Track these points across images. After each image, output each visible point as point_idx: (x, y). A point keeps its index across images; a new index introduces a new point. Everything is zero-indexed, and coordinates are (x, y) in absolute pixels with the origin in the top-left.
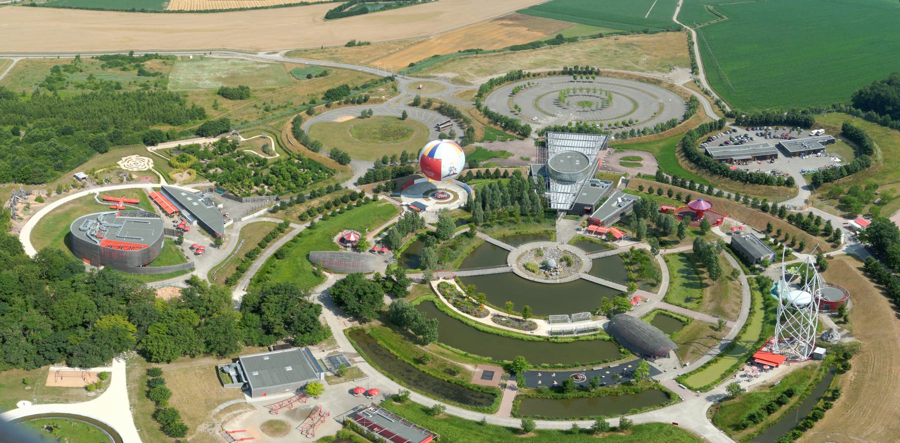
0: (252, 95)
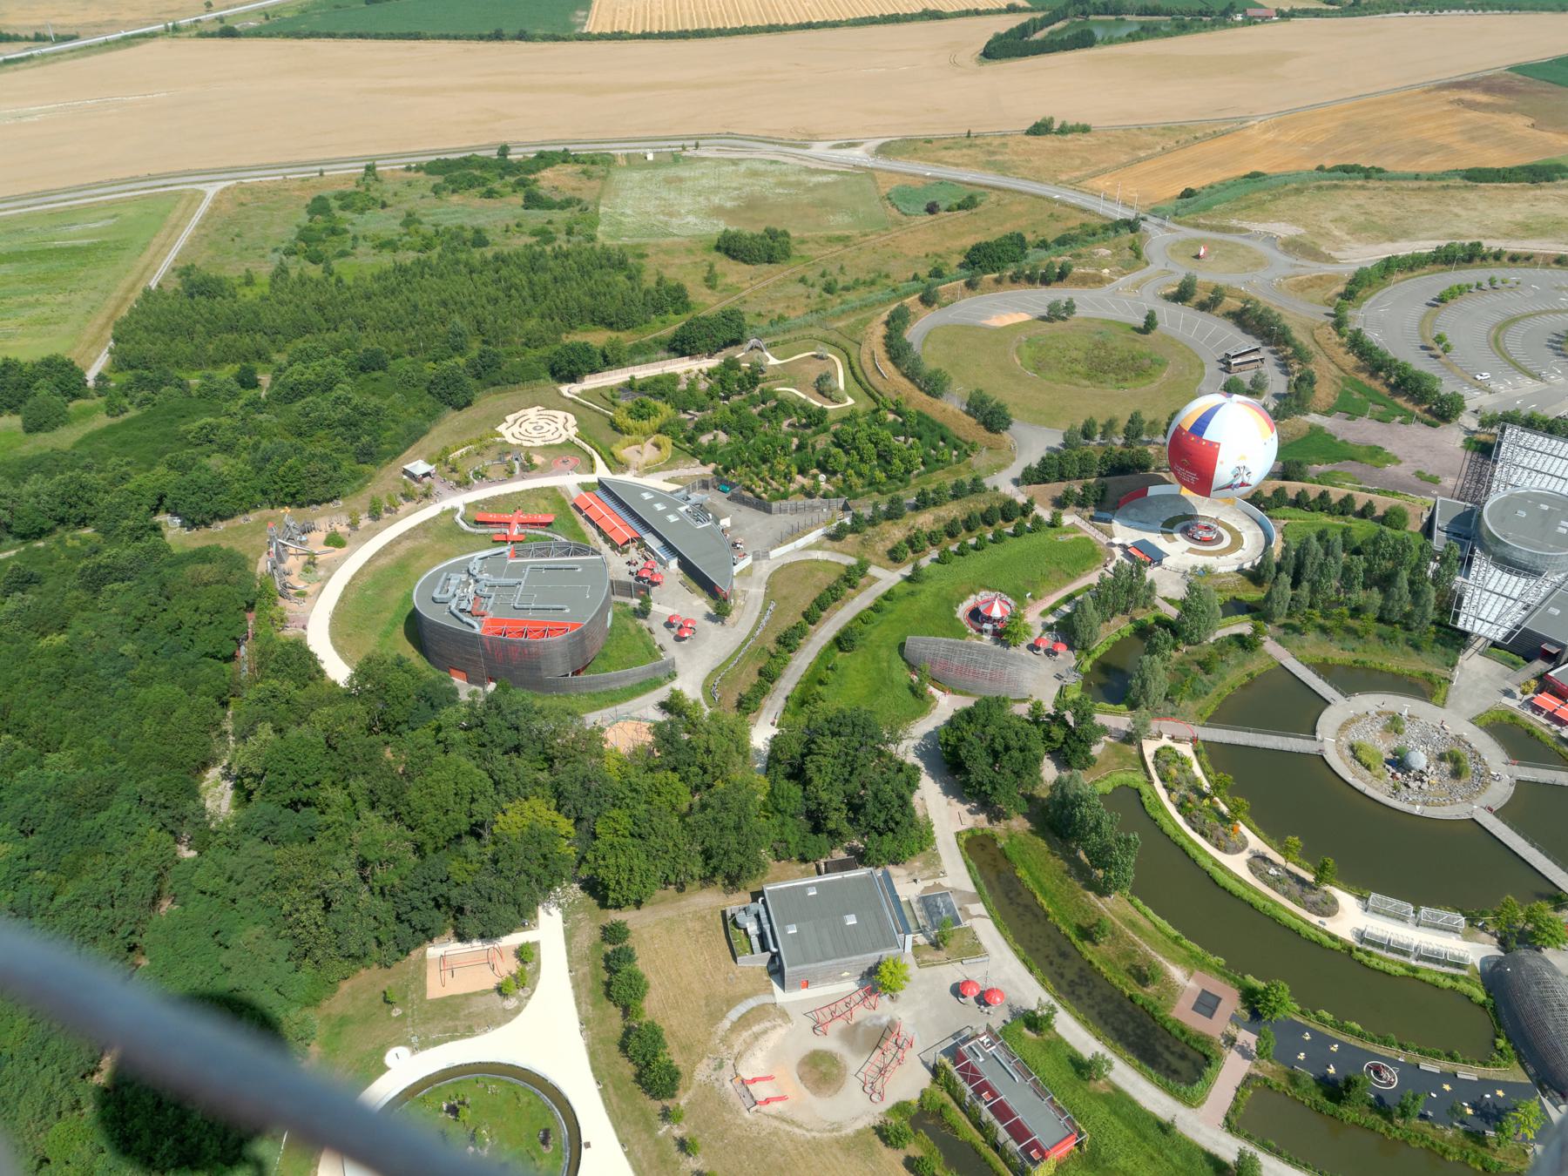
0: (794, 253)
